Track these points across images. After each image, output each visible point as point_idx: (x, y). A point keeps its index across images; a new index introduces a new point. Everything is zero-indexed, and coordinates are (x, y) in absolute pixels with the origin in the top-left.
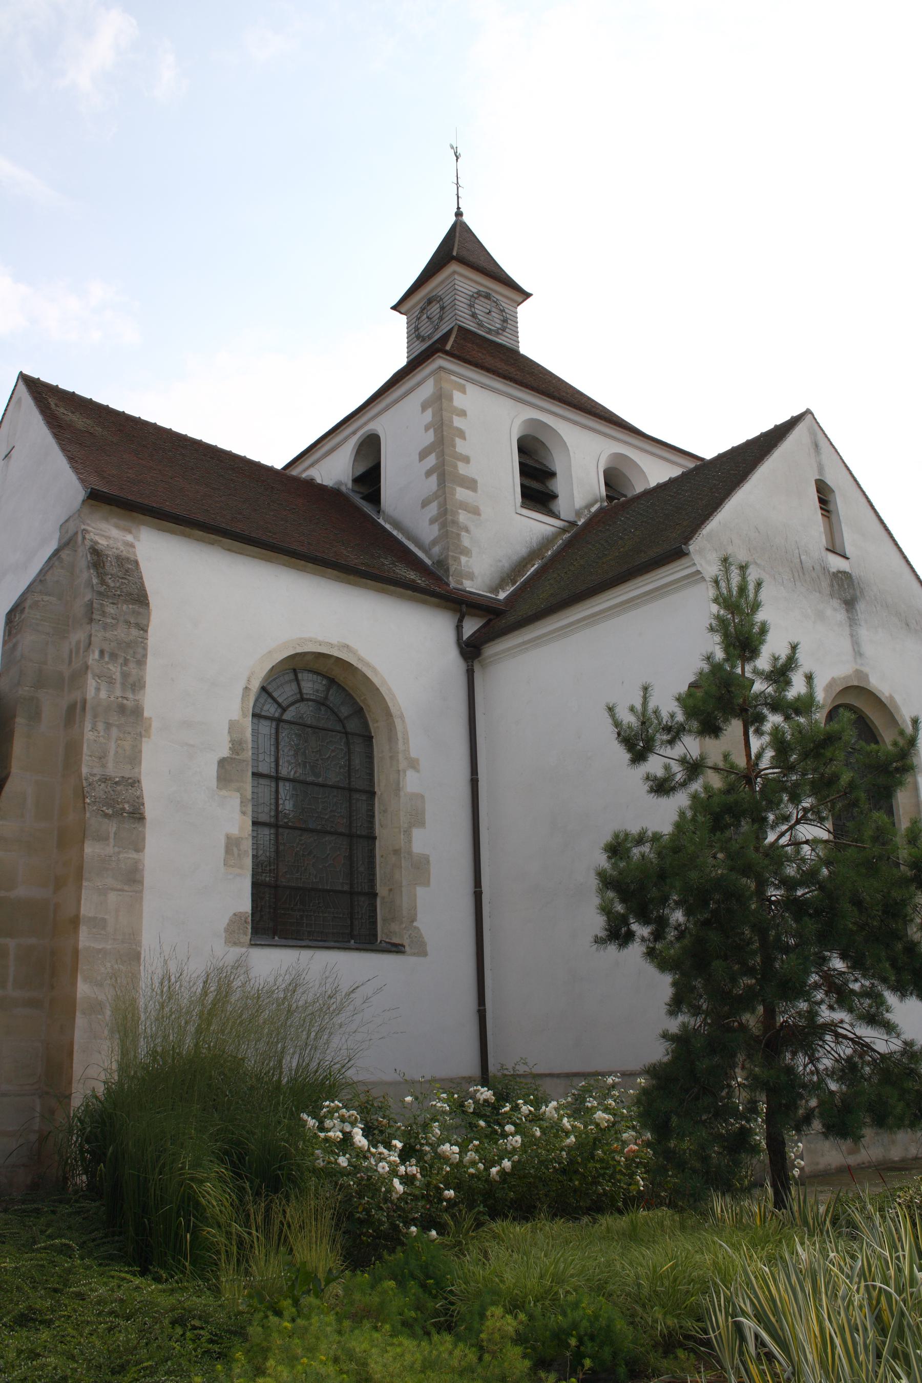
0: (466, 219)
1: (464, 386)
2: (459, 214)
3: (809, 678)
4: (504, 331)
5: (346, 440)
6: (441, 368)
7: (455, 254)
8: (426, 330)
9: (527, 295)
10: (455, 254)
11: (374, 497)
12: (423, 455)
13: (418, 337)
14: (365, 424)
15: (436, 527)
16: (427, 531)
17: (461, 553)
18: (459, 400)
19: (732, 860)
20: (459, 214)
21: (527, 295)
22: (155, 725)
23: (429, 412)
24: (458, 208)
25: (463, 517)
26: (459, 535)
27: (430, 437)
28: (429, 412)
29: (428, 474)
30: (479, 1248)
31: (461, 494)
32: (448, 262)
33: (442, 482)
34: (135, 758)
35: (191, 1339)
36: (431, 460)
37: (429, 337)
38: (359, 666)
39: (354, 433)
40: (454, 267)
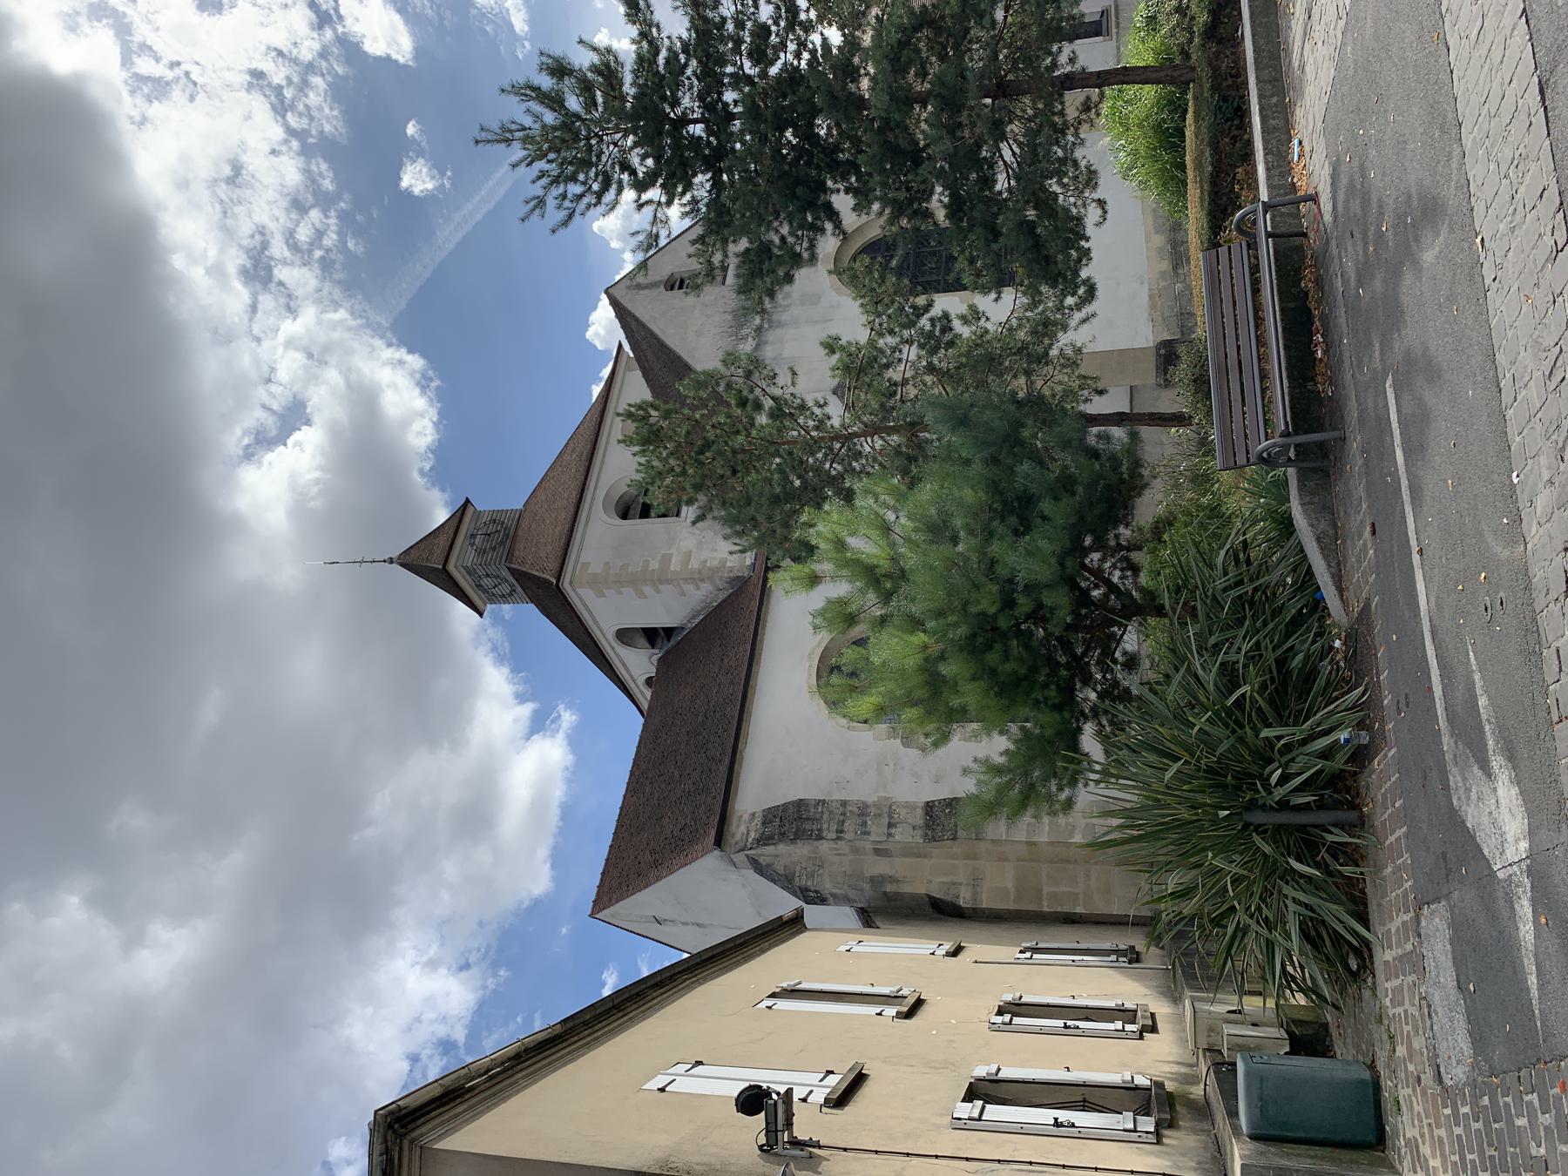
0: (395, 555)
1: (583, 564)
2: (391, 561)
3: (669, 37)
4: (503, 523)
5: (617, 655)
6: (571, 583)
7: (441, 567)
8: (505, 589)
9: (467, 501)
10: (441, 567)
11: (669, 632)
12: (642, 595)
13: (510, 595)
14: (607, 640)
15: (702, 585)
16: (706, 588)
17: (724, 566)
18: (596, 568)
19: (974, 226)
20: (391, 561)
21: (467, 501)
22: (882, 794)
23: (607, 592)
24: (385, 561)
25: (694, 564)
26: (709, 569)
27: (628, 592)
28: (607, 592)
29: (658, 591)
30: (1313, 53)
31: (675, 565)
32: (447, 571)
33: (668, 582)
34: (910, 806)
35: (1088, 98)
36: (648, 590)
37: (512, 586)
38: (824, 645)
39: (613, 648)
40: (451, 568)
